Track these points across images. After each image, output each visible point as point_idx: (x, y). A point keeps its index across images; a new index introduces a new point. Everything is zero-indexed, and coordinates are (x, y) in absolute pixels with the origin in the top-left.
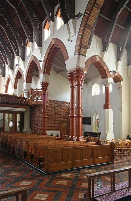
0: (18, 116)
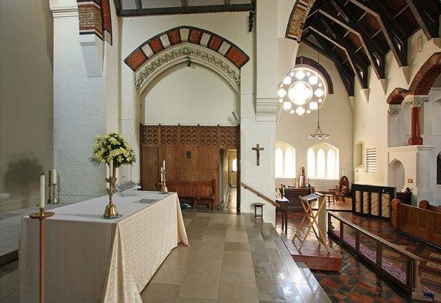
0: (298, 5)
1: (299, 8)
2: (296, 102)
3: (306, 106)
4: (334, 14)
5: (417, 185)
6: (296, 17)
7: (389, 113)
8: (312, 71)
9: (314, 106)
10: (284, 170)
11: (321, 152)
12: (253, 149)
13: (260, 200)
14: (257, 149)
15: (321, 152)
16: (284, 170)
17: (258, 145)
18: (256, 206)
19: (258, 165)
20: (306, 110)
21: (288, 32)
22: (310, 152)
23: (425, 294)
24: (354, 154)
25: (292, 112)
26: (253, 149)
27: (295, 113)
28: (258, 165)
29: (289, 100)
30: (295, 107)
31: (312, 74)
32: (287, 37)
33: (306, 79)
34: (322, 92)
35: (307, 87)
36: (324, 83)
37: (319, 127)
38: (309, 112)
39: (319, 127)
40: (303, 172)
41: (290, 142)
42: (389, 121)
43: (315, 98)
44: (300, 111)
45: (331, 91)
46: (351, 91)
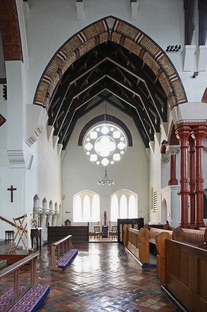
0: (43, 79)
1: (44, 82)
2: (102, 155)
3: (110, 158)
4: (122, 81)
5: (171, 218)
6: (42, 88)
7: (162, 161)
8: (116, 127)
9: (117, 157)
10: (91, 215)
11: (124, 198)
12: (8, 189)
13: (11, 228)
14: (12, 189)
15: (124, 198)
16: (91, 215)
17: (12, 186)
18: (8, 232)
19: (12, 201)
20: (110, 161)
21: (35, 100)
22: (114, 198)
23: (59, 267)
24: (147, 200)
25: (98, 163)
26: (8, 189)
27: (101, 164)
28: (12, 201)
29: (95, 153)
30: (100, 158)
31: (100, 128)
32: (34, 103)
33: (110, 134)
34: (123, 145)
35: (99, 141)
36: (124, 138)
37: (106, 175)
38: (112, 163)
39: (106, 175)
40: (105, 215)
41: (95, 190)
42: (162, 167)
43: (117, 151)
44: (105, 162)
45: (130, 144)
46: (148, 146)
